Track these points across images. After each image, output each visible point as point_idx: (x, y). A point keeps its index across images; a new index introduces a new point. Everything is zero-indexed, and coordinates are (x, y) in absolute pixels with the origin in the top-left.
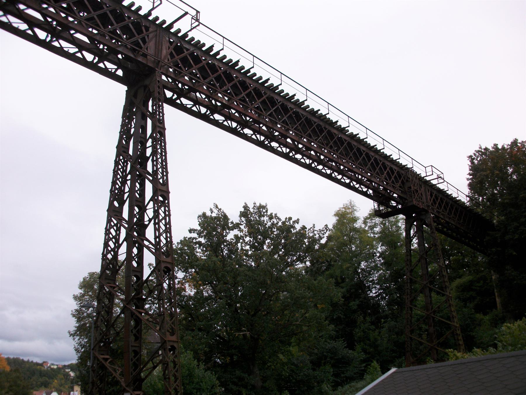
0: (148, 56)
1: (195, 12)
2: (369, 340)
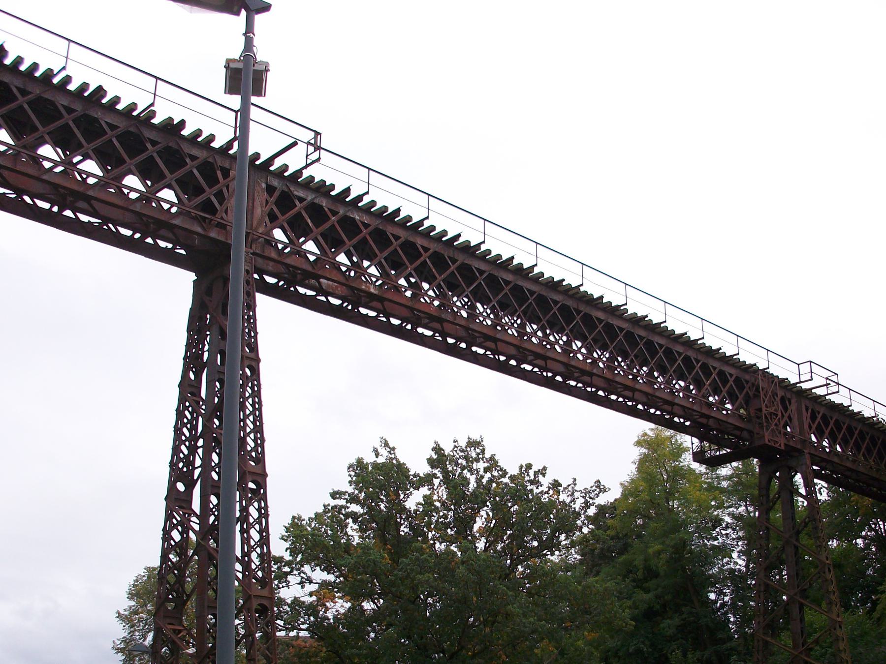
0: (228, 227)
1: (313, 134)
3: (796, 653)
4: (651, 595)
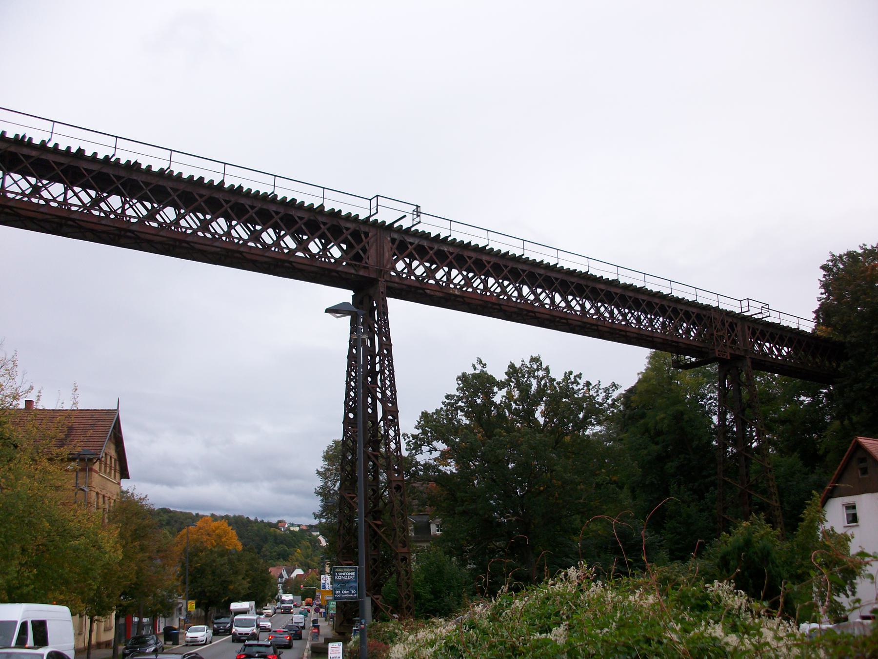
1: (415, 207)
3: (743, 488)
4: (659, 447)
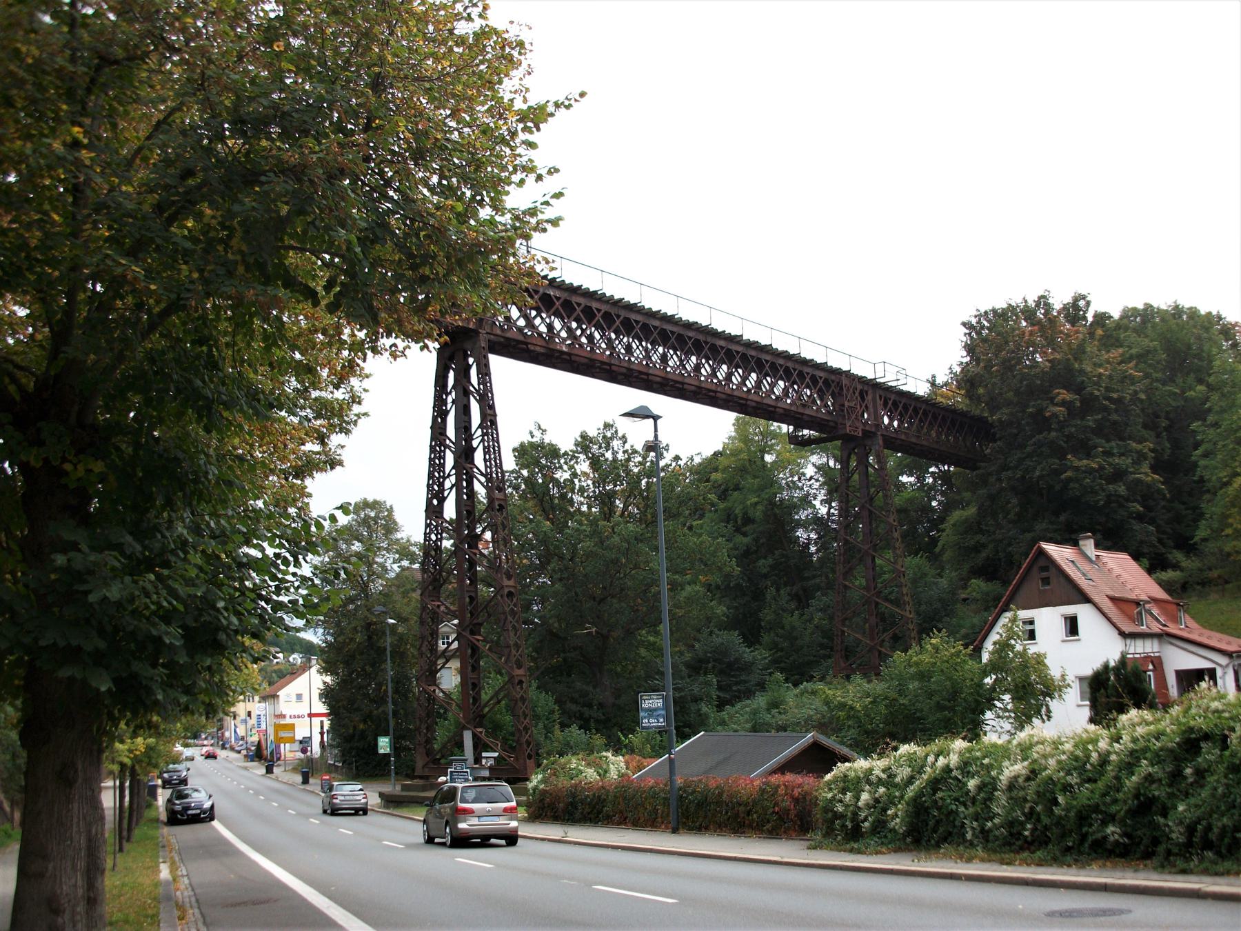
2: (783, 628)
